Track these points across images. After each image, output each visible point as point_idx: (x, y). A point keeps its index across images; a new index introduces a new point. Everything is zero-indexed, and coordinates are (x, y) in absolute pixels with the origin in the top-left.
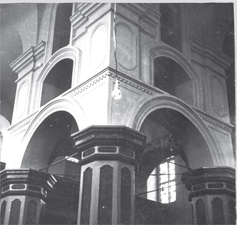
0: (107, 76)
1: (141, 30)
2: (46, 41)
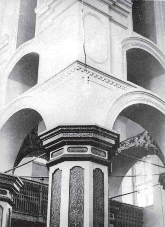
0: (75, 70)
1: (111, 19)
2: (10, 34)
